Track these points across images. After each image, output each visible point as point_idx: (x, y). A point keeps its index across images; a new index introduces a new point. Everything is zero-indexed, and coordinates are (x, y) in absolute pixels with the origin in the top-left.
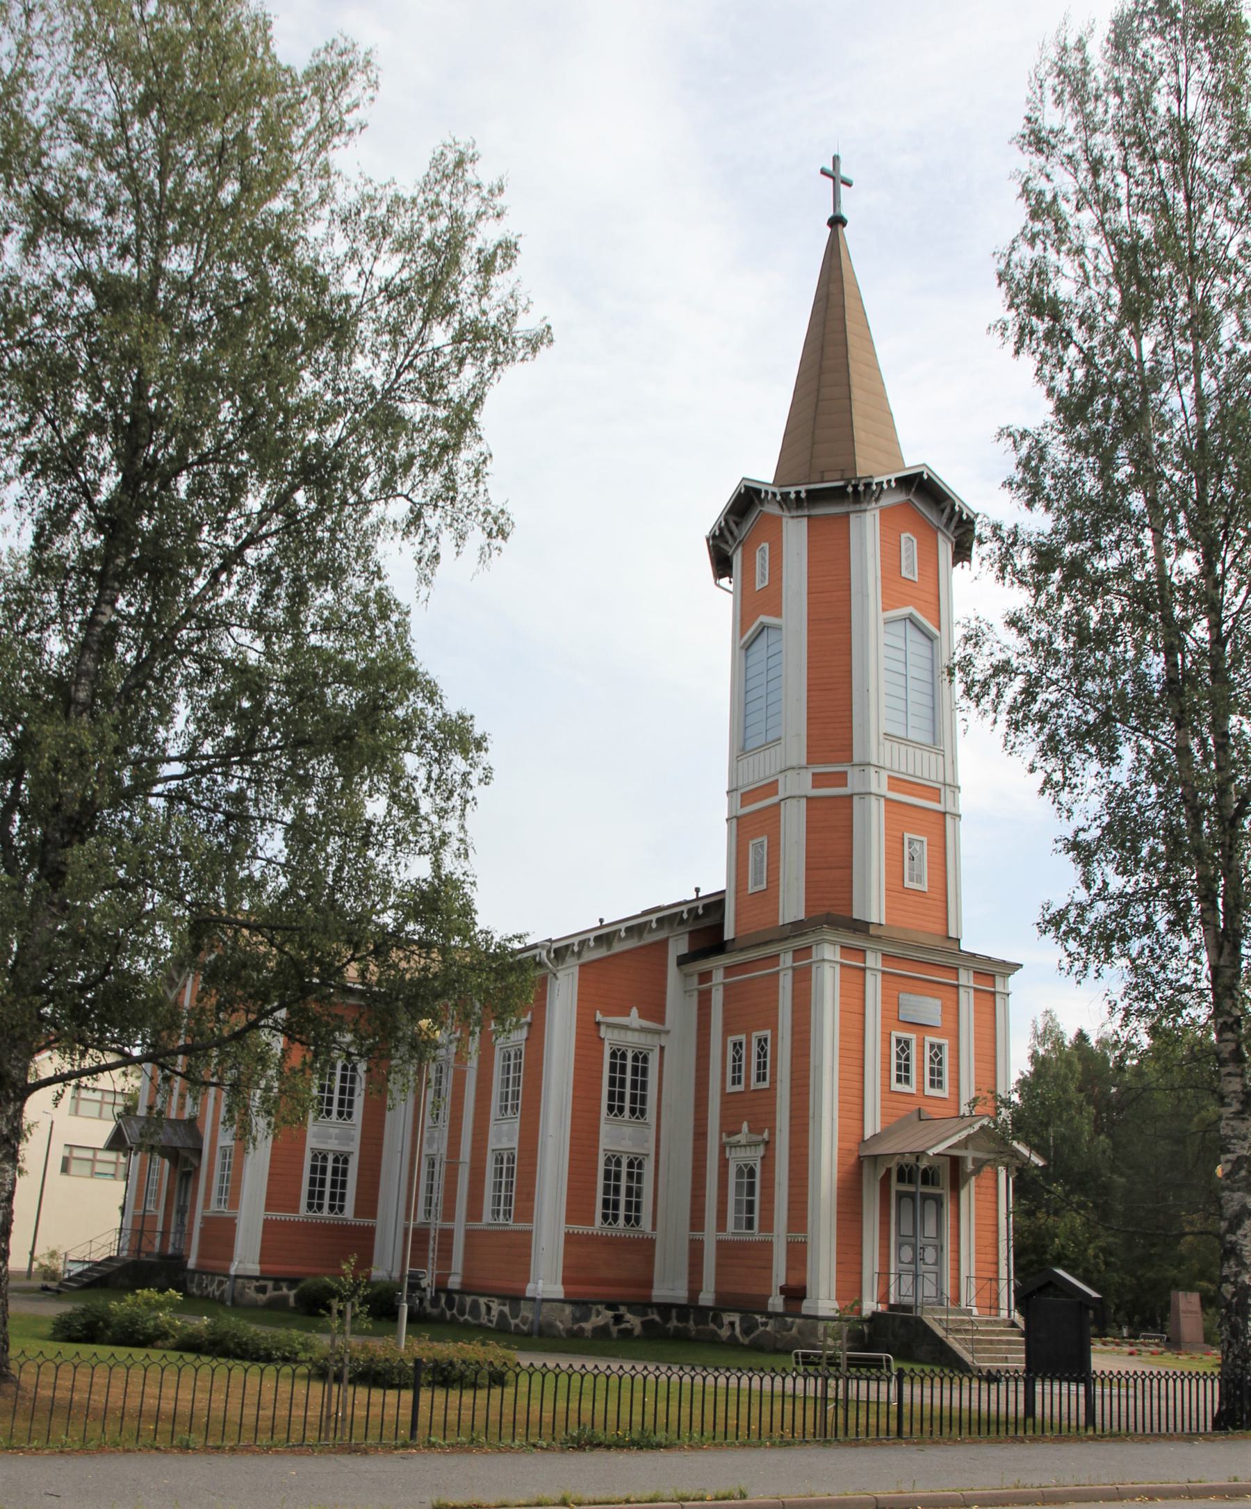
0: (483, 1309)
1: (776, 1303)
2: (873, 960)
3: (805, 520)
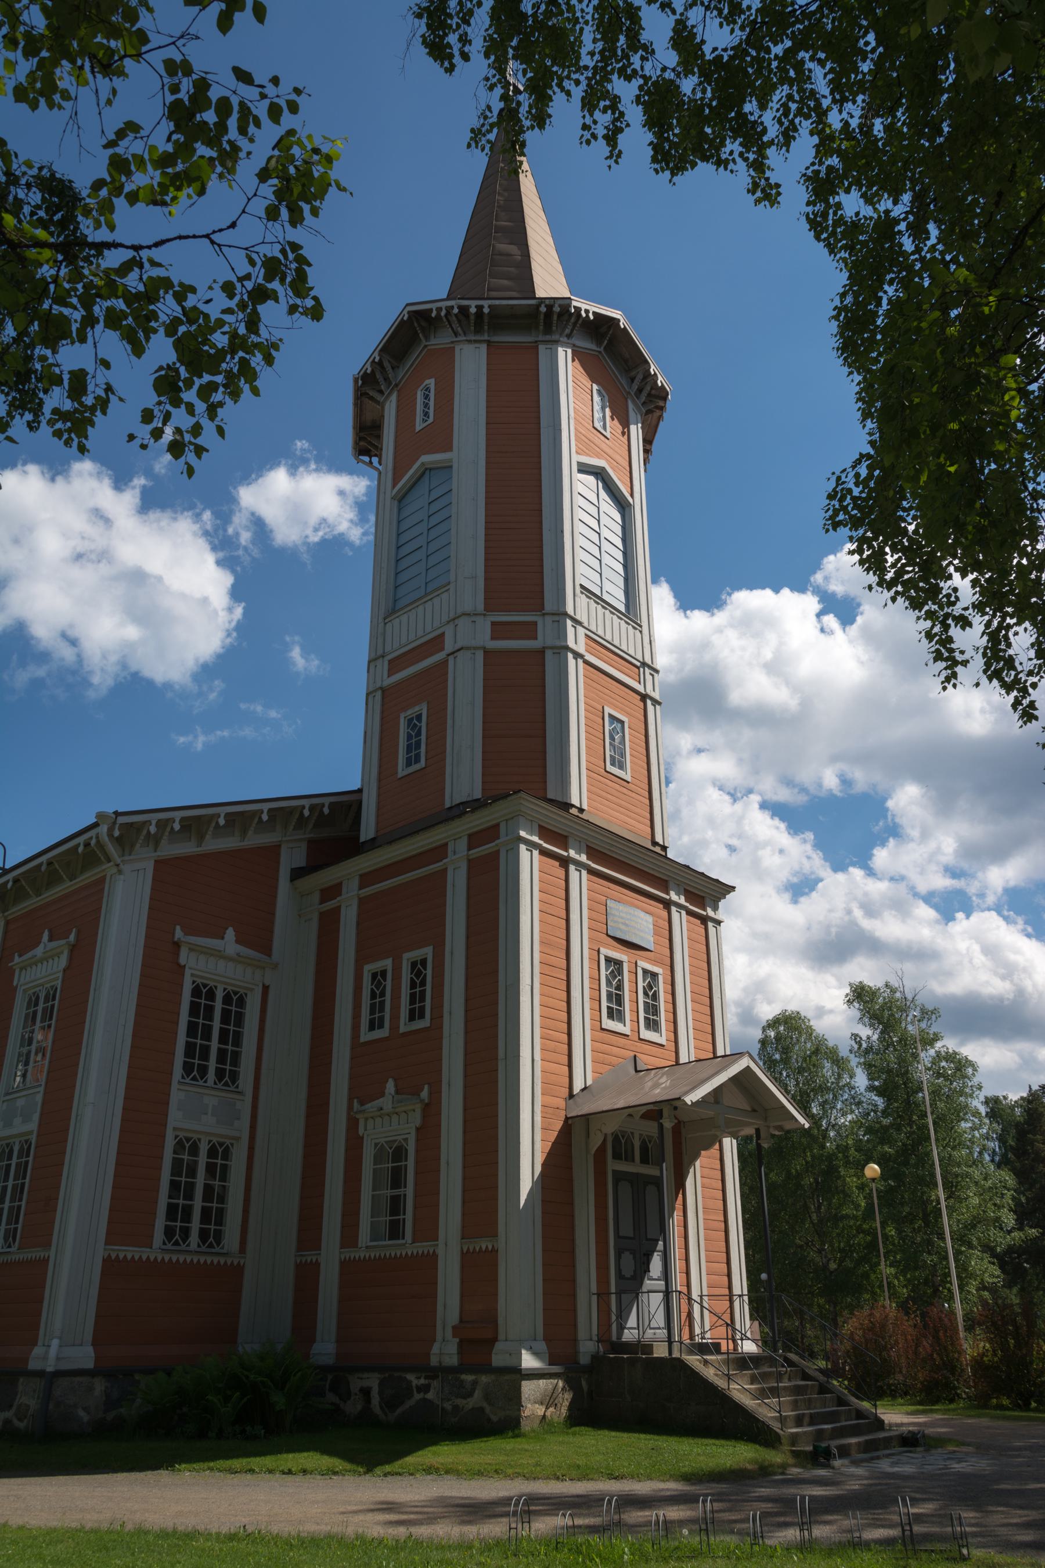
3: (484, 348)
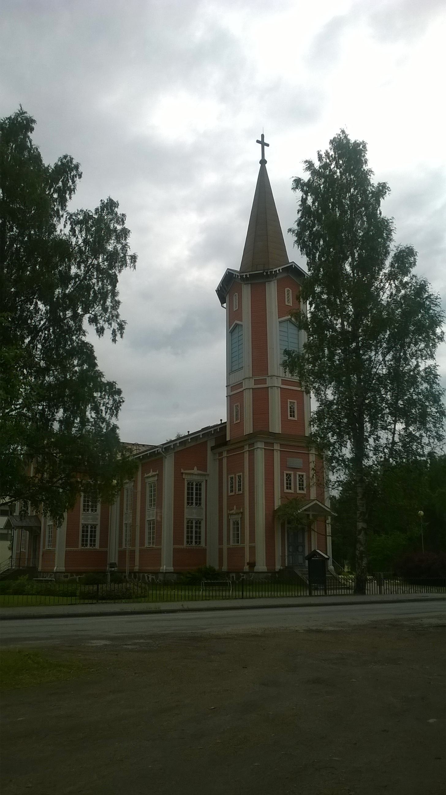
0: (146, 577)
1: (246, 568)
2: (277, 447)
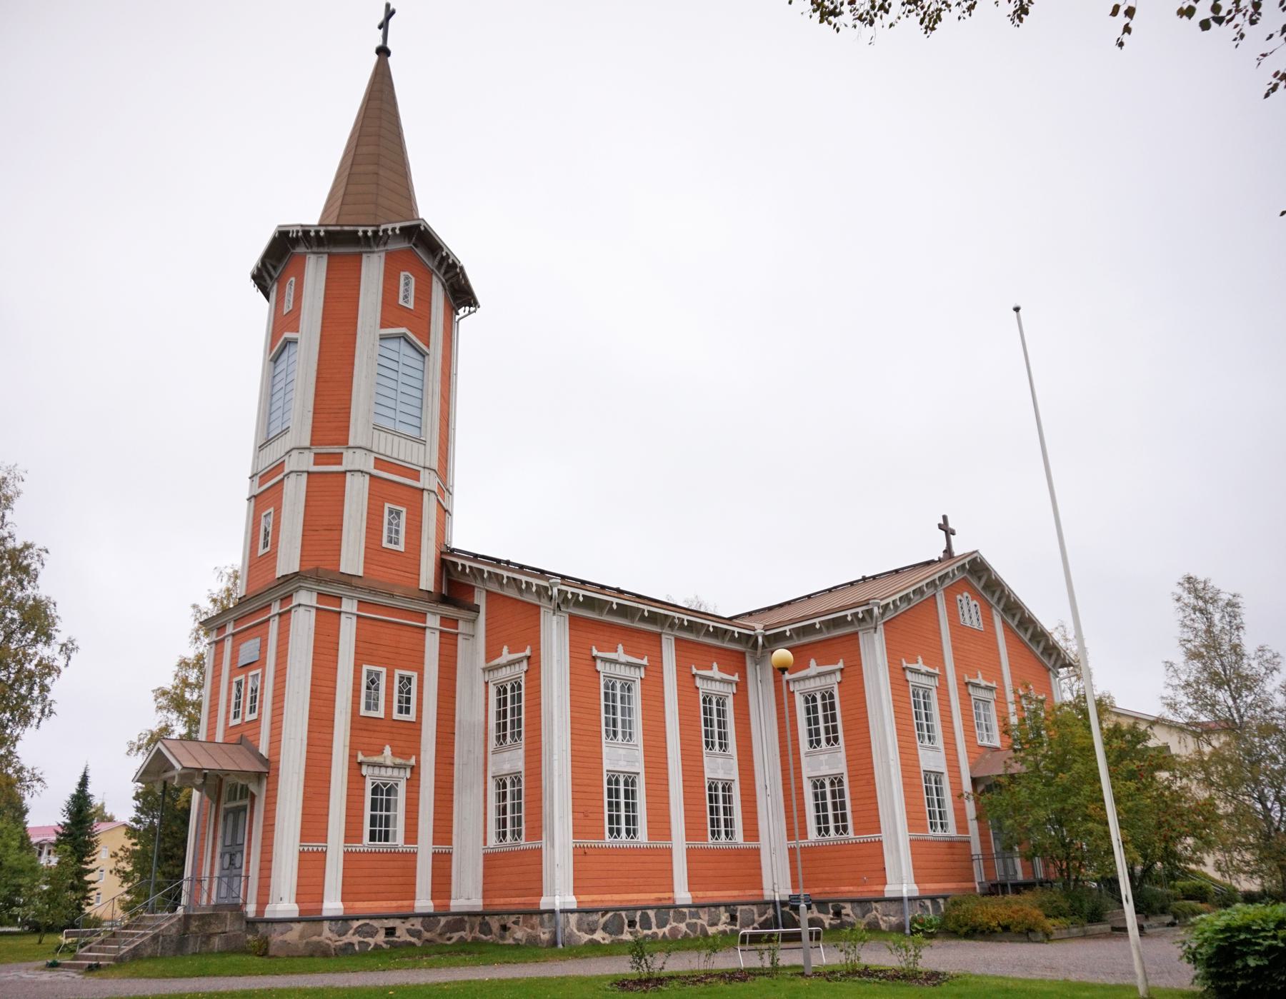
2: (349, 606)
3: (326, 257)
